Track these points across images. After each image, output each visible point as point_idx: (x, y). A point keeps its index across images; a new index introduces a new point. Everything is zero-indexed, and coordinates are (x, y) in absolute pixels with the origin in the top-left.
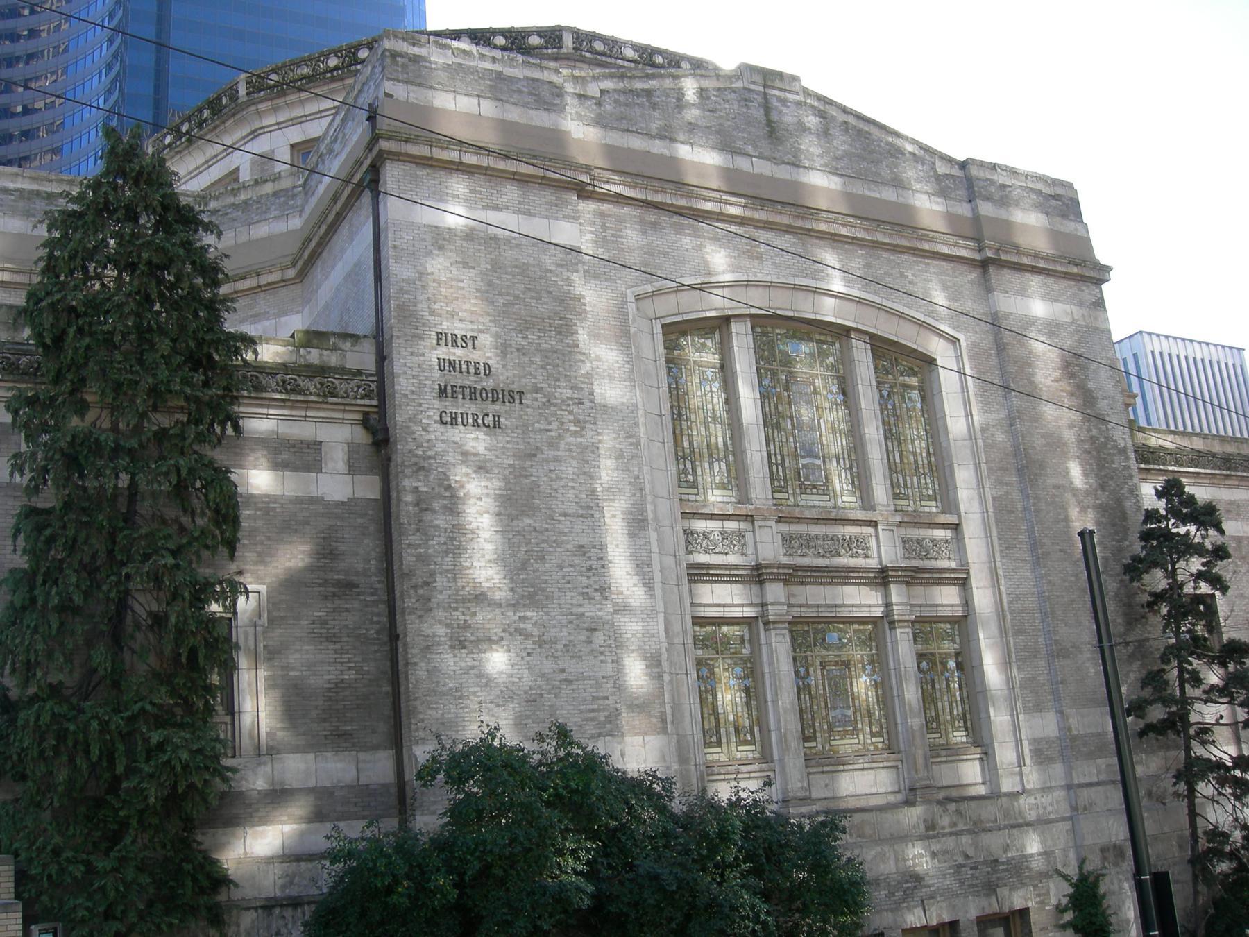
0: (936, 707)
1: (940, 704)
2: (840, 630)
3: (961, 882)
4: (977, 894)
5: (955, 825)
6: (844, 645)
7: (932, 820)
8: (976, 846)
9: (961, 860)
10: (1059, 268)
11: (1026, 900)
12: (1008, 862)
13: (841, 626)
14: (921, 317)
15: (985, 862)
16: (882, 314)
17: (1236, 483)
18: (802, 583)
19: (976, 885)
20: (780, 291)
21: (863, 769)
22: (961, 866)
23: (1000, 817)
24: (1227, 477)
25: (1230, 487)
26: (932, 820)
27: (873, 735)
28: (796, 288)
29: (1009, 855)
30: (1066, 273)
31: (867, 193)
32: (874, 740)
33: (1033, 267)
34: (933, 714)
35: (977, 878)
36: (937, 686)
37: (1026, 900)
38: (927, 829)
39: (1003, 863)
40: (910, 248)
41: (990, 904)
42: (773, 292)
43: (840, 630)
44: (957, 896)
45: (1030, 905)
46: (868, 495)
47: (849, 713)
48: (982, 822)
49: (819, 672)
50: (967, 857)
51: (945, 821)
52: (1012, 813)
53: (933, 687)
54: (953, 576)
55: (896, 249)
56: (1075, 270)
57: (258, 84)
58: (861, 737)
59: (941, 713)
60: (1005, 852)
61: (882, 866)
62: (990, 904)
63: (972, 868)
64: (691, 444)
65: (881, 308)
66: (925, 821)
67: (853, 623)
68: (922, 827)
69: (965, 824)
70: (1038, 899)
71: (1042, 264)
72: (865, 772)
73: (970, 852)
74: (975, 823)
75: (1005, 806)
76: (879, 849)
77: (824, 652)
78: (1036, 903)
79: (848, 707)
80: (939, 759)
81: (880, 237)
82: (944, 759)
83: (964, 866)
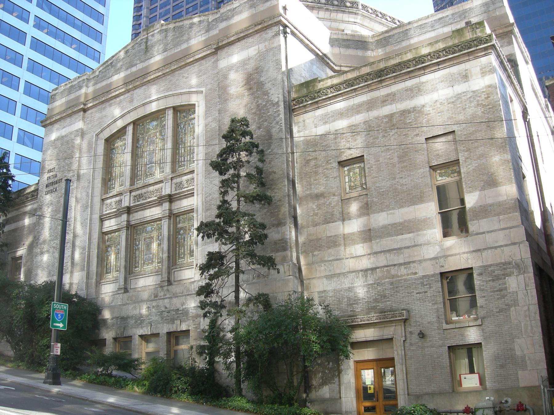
0: (184, 248)
1: (186, 247)
2: (152, 225)
3: (162, 318)
4: (168, 323)
5: (165, 295)
6: (153, 231)
7: (157, 293)
8: (170, 303)
9: (163, 309)
10: (251, 31)
11: (189, 326)
12: (183, 310)
13: (152, 224)
14: (187, 90)
15: (173, 310)
16: (175, 97)
17: (393, 81)
18: (136, 212)
19: (168, 319)
20: (140, 109)
21: (149, 276)
22: (163, 311)
23: (185, 291)
24: (381, 81)
25: (387, 86)
26: (157, 293)
27: (158, 263)
28: (144, 105)
29: (184, 307)
30: (256, 31)
31: (176, 51)
32: (158, 265)
33: (238, 39)
34: (183, 251)
35: (169, 317)
36: (186, 240)
37: (189, 326)
38: (155, 297)
39: (181, 311)
40: (186, 64)
41: (173, 327)
42: (138, 110)
43: (152, 225)
44: (160, 323)
45: (190, 329)
46: (132, 172)
47: (151, 256)
48: (177, 294)
49: (143, 243)
50: (166, 308)
51: (162, 294)
52: (190, 289)
53: (184, 240)
54: (189, 193)
55: (181, 68)
56: (260, 27)
57: (381, 42)
58: (154, 264)
59: (186, 250)
60: (182, 306)
61: (134, 311)
62: (173, 327)
63: (167, 313)
64: (115, 174)
65: (173, 95)
66: (154, 294)
67: (157, 221)
68: (153, 296)
69: (170, 295)
70: (194, 326)
71: (242, 35)
72: (150, 277)
73: (168, 306)
74: (174, 294)
75: (187, 286)
76: (134, 305)
77: (146, 235)
78: (193, 328)
79: (151, 254)
80: (177, 269)
81: (173, 68)
82: (179, 269)
83: (165, 311)
